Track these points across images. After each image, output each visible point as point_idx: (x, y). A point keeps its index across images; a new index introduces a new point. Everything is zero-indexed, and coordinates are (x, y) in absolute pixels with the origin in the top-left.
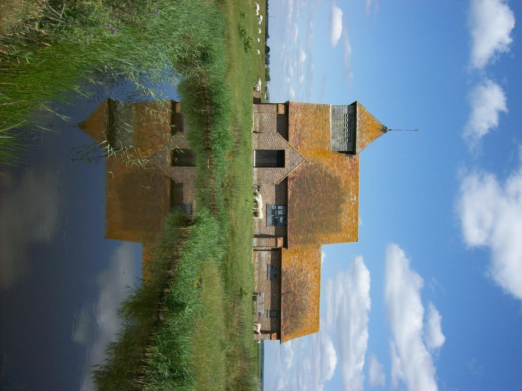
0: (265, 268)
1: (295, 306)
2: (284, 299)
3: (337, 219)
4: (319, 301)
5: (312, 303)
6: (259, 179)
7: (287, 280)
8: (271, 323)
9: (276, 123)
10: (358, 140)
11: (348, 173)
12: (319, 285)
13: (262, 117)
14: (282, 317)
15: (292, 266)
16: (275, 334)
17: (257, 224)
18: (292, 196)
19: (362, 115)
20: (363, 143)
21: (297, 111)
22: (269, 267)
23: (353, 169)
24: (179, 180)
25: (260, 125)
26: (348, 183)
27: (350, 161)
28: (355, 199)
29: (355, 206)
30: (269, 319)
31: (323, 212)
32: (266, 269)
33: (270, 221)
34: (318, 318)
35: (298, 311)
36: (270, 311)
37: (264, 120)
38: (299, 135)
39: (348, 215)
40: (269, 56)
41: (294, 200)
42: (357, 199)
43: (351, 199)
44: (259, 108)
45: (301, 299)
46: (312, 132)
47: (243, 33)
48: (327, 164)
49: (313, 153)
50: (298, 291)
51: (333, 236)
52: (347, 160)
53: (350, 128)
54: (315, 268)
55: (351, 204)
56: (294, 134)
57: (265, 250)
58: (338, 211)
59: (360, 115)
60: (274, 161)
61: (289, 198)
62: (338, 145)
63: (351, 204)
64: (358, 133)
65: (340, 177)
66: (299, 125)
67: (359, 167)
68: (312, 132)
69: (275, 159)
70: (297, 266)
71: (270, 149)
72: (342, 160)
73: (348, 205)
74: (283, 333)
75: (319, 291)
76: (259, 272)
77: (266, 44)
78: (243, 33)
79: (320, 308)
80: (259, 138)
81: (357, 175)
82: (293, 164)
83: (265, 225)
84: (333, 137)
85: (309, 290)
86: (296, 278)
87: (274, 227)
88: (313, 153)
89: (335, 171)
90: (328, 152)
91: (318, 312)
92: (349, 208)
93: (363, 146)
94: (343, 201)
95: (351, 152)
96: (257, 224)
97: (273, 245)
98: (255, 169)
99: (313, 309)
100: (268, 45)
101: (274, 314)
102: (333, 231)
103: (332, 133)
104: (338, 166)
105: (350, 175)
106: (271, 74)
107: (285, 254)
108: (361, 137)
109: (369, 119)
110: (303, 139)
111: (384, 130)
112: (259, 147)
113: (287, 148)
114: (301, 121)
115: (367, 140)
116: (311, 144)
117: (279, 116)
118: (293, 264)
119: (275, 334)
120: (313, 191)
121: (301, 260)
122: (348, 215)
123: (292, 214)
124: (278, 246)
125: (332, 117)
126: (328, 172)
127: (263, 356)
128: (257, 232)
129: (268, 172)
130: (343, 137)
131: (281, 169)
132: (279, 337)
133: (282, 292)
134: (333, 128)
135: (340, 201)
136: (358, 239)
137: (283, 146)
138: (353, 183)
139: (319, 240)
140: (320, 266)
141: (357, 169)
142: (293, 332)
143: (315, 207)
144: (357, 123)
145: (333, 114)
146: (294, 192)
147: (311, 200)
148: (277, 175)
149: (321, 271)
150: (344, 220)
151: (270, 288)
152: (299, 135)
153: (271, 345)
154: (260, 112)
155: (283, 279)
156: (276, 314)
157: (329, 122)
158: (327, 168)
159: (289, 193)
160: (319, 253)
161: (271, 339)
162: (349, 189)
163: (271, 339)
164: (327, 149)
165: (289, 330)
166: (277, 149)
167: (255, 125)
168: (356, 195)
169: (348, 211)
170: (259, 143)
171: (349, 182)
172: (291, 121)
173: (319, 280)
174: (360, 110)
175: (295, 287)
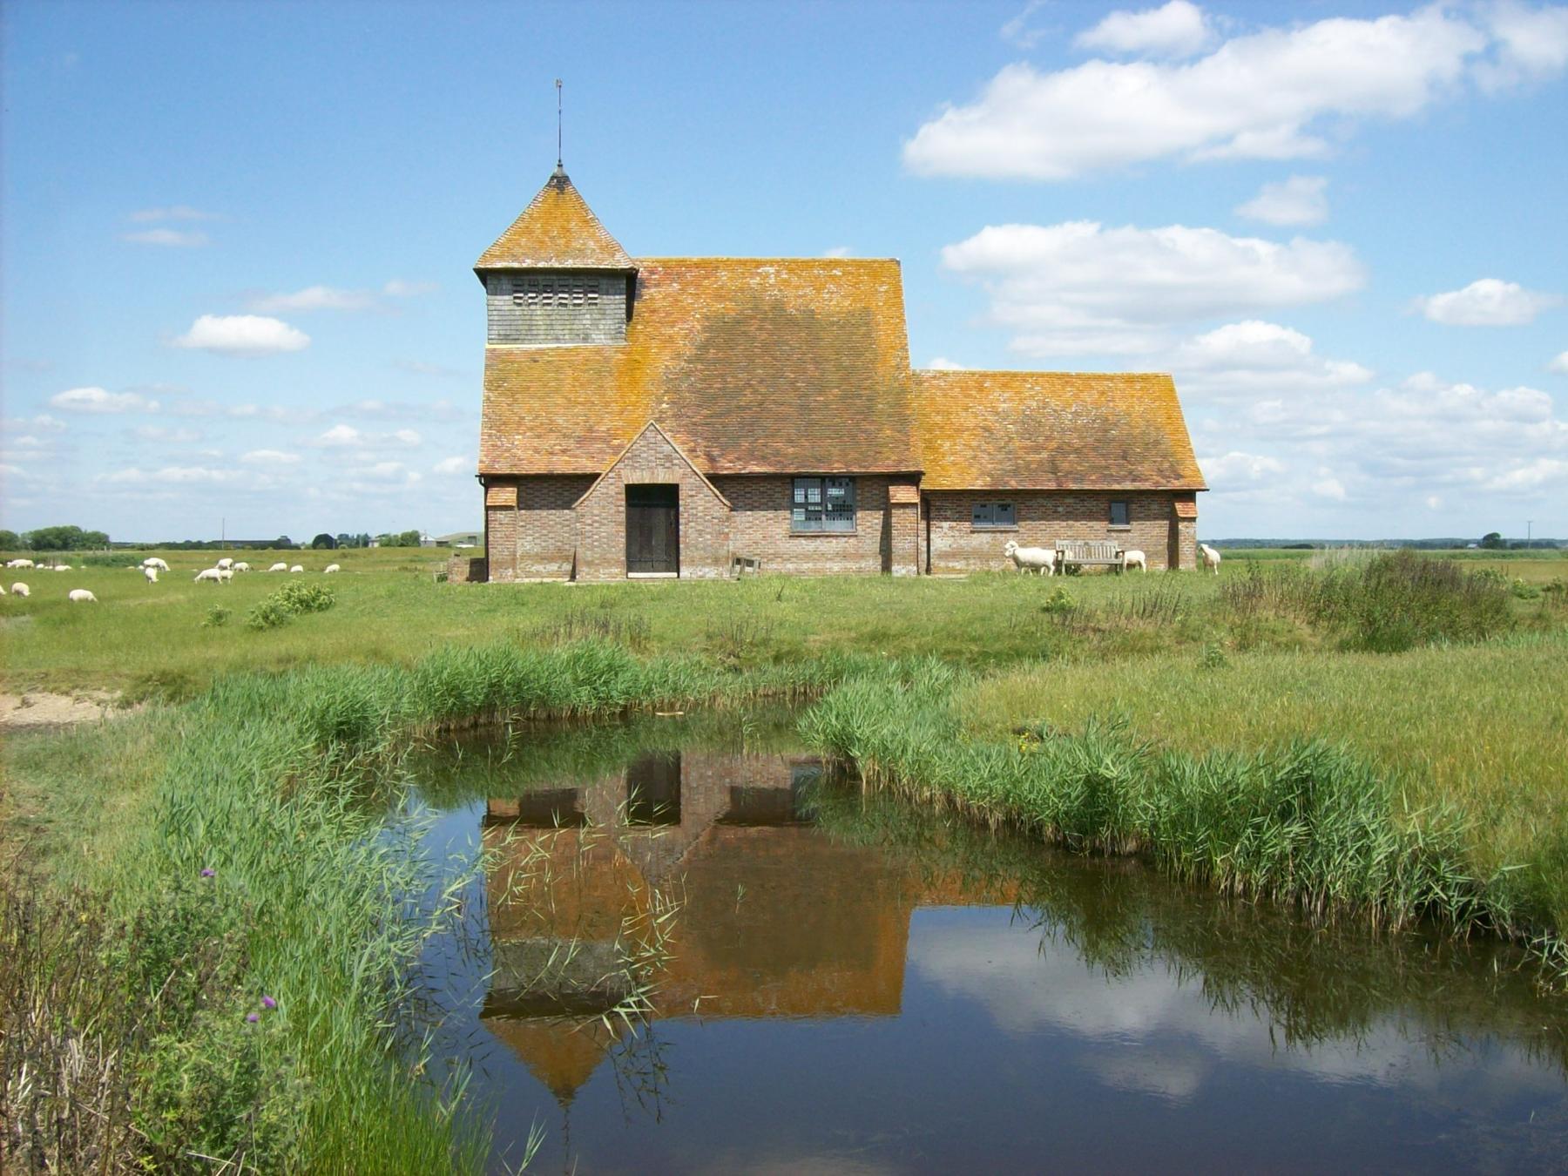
0: (982, 540)
1: (1095, 449)
2: (1075, 480)
3: (833, 324)
4: (1078, 376)
5: (1085, 396)
6: (716, 561)
7: (1016, 472)
8: (1147, 518)
9: (544, 513)
10: (591, 263)
11: (692, 290)
12: (1032, 375)
13: (527, 556)
15: (974, 457)
16: (1178, 506)
18: (763, 459)
19: (517, 251)
20: (601, 248)
22: (978, 526)
24: (598, 488)
25: (551, 560)
26: (723, 292)
28: (772, 270)
29: (791, 271)
30: (1134, 525)
31: (811, 367)
32: (985, 538)
33: (840, 526)
34: (1130, 379)
35: (1107, 440)
36: (1112, 521)
37: (537, 549)
38: (581, 441)
39: (818, 291)
40: (343, 537)
41: (777, 453)
42: (771, 263)
43: (772, 281)
44: (501, 565)
45: (1076, 430)
47: (272, 617)
51: (882, 335)
52: (652, 295)
53: (556, 287)
54: (981, 389)
55: (786, 282)
56: (575, 456)
57: (928, 540)
58: (809, 322)
59: (515, 257)
60: (660, 516)
61: (771, 470)
62: (609, 324)
63: (785, 280)
64: (569, 264)
66: (551, 441)
67: (674, 257)
68: (571, 403)
69: (652, 512)
70: (974, 443)
71: (623, 529)
72: (654, 311)
73: (790, 293)
74: (1177, 484)
75: (1050, 375)
78: (272, 617)
80: (589, 564)
81: (697, 265)
82: (668, 458)
83: (852, 540)
84: (585, 339)
87: (859, 514)
88: (633, 398)
89: (686, 332)
91: (1111, 378)
92: (797, 288)
93: (611, 248)
94: (778, 306)
95: (628, 282)
98: (685, 572)
99: (1103, 393)
101: (1118, 509)
102: (867, 335)
103: (572, 341)
104: (673, 324)
106: (397, 530)
108: (581, 253)
109: (528, 231)
110: (590, 430)
111: (560, 182)
113: (619, 476)
114: (539, 437)
115: (592, 236)
116: (607, 404)
117: (523, 503)
118: (970, 453)
119: (1178, 506)
120: (748, 397)
121: (957, 430)
122: (818, 291)
124: (917, 500)
125: (523, 341)
128: (874, 564)
129: (692, 535)
130: (584, 309)
131: (683, 494)
132: (1188, 495)
133: (1053, 486)
134: (557, 340)
135: (778, 318)
137: (612, 490)
138: (724, 275)
139: (896, 379)
140: (973, 374)
141: (681, 263)
144: (541, 265)
147: (775, 402)
148: (700, 507)
150: (833, 301)
151: (1042, 525)
152: (581, 441)
153: (1209, 521)
154: (513, 562)
156: (1117, 506)
157: (541, 352)
159: (757, 469)
161: (1193, 519)
162: (742, 290)
164: (620, 356)
165: (1166, 465)
166: (623, 509)
168: (757, 267)
170: (606, 562)
172: (539, 467)
173: (1015, 375)
174: (501, 257)
175: (1037, 449)
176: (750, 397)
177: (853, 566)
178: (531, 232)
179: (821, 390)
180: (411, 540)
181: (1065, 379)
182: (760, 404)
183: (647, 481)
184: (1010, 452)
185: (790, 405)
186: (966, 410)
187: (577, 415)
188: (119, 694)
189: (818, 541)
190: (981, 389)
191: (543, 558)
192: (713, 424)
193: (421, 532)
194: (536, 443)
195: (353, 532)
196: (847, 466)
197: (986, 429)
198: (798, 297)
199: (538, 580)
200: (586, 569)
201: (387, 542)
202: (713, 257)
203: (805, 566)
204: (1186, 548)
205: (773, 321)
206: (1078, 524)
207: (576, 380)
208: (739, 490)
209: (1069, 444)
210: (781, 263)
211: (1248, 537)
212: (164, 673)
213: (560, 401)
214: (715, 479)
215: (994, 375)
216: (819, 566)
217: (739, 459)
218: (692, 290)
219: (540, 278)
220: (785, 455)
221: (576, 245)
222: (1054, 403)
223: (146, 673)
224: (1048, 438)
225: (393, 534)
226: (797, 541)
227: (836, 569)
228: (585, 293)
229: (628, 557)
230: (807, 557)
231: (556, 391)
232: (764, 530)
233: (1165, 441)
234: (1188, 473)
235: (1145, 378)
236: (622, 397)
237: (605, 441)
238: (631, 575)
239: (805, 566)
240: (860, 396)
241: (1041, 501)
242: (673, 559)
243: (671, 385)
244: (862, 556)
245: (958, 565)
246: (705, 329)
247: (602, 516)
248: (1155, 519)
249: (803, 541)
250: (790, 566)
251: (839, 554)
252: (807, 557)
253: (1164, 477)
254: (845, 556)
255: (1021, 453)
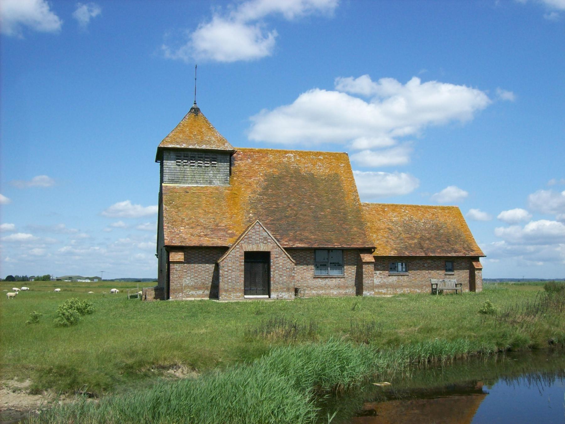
0: (393, 279)
1: (435, 238)
2: (432, 252)
3: (322, 180)
4: (422, 206)
5: (426, 215)
6: (288, 290)
7: (406, 248)
8: (461, 269)
9: (196, 265)
10: (214, 147)
11: (257, 163)
12: (404, 206)
13: (187, 286)
14: (454, 255)
15: (387, 242)
16: (474, 263)
17: (341, 291)
18: (301, 241)
19: (178, 140)
20: (218, 140)
21: (178, 234)
22: (392, 273)
23: (251, 157)
25: (199, 288)
26: (272, 164)
27: (241, 160)
28: (292, 155)
29: (300, 156)
30: (456, 272)
31: (316, 199)
32: (395, 278)
33: (335, 273)
34: (443, 209)
35: (438, 234)
36: (446, 270)
37: (192, 283)
38: (213, 230)
39: (314, 165)
40: (17, 277)
41: (307, 238)
42: (292, 152)
43: (293, 160)
44: (176, 291)
45: (426, 230)
46: (206, 213)
47: (72, 319)
48: (249, 191)
49: (236, 211)
50: (416, 233)
51: (345, 185)
52: (240, 164)
53: (197, 158)
54: (384, 212)
55: (299, 161)
56: (212, 238)
58: (311, 179)
59: (178, 143)
60: (259, 268)
61: (306, 246)
62: (221, 176)
63: (298, 160)
64: (204, 147)
65: (265, 175)
66: (198, 230)
67: (248, 148)
68: (206, 213)
69: (257, 266)
70: (386, 235)
71: (243, 273)
72: (241, 171)
73: (301, 165)
74: (472, 254)
75: (411, 206)
76: (399, 287)
77: (4, 280)
78: (72, 319)
79: (430, 205)
80: (226, 291)
81: (259, 152)
82: (265, 239)
83: (342, 279)
84: (210, 183)
85: (412, 219)
86: (401, 237)
87: (345, 267)
88: (236, 211)
89: (257, 181)
90: (231, 190)
91: (435, 208)
92: (304, 163)
93: (222, 141)
94: (297, 171)
95: (228, 156)
96: (341, 291)
97: (371, 267)
98: (274, 295)
99: (433, 214)
100: (5, 278)
101: (449, 265)
102: (338, 185)
103: (204, 183)
104: (250, 177)
105: (260, 161)
106: (42, 275)
107: (379, 252)
108: (209, 142)
109: (182, 131)
110: (217, 225)
112: (239, 291)
114: (192, 228)
115: (213, 135)
116: (224, 214)
117: (187, 261)
118: (385, 240)
119: (474, 263)
120: (289, 212)
121: (378, 229)
122: (314, 165)
123: (326, 242)
125: (180, 183)
126: (259, 190)
127: (528, 280)
128: (352, 291)
129: (277, 276)
130: (210, 169)
131: (273, 256)
132: (476, 259)
133: (423, 255)
134: (197, 183)
135: (297, 175)
136: (345, 153)
137: (238, 254)
138: (271, 157)
139: (355, 205)
140: (380, 205)
141: (251, 150)
142: (468, 243)
143: (311, 209)
144: (190, 147)
145: (176, 182)
146: (295, 239)
147: (302, 214)
148: (280, 263)
149: (386, 203)
150: (321, 170)
151: (418, 272)
152: (213, 230)
153: (488, 269)
154: (181, 290)
155: (407, 254)
156: (449, 264)
157: (188, 188)
158: (254, 192)
159: (300, 245)
160: (364, 206)
161: (481, 269)
162: (280, 163)
163: (481, 269)
164: (227, 191)
165: (466, 246)
166: (243, 263)
167: (199, 296)
168: (286, 154)
169: (309, 165)
170: (234, 290)
171: (270, 162)
172: (194, 242)
173: (396, 206)
174: (171, 143)
175: (412, 238)
176: (290, 212)
177: (343, 292)
178: (184, 132)
179: (322, 209)
180: (47, 278)
181: (417, 208)
182: (295, 216)
183: (255, 250)
184: (401, 240)
185: (309, 216)
186: (380, 220)
187: (210, 219)
188: (27, 383)
189: (327, 280)
190: (384, 212)
191: (195, 288)
192: (275, 224)
193: (51, 275)
194: (191, 230)
195: (21, 275)
196: (341, 245)
197: (389, 229)
198: (305, 167)
199: (199, 299)
200: (224, 293)
201: (38, 279)
202: (265, 149)
203: (321, 292)
204: (478, 282)
205: (296, 178)
206: (433, 272)
207: (208, 201)
208: (299, 255)
209: (425, 236)
210: (296, 152)
211: (527, 277)
212: (60, 367)
213: (201, 211)
214: (289, 250)
215: (388, 205)
216: (327, 291)
217: (290, 240)
218: (257, 163)
219: (189, 153)
220: (311, 239)
221: (207, 139)
222: (415, 218)
223: (46, 367)
224: (416, 233)
225: (40, 276)
226: (317, 280)
227: (335, 293)
228: (211, 161)
229: (245, 286)
230: (322, 288)
231: (198, 207)
232: (306, 274)
233: (460, 234)
234: (475, 249)
235: (449, 208)
236: (230, 210)
237: (224, 230)
238: (246, 296)
239: (321, 292)
240: (340, 213)
241: (417, 261)
242: (267, 289)
243: (253, 205)
244: (347, 287)
245: (384, 291)
246: (265, 180)
247: (233, 267)
248: (464, 269)
249: (320, 280)
250: (314, 292)
251: (335, 286)
252: (322, 288)
253: (466, 251)
254: (339, 287)
255: (406, 240)
